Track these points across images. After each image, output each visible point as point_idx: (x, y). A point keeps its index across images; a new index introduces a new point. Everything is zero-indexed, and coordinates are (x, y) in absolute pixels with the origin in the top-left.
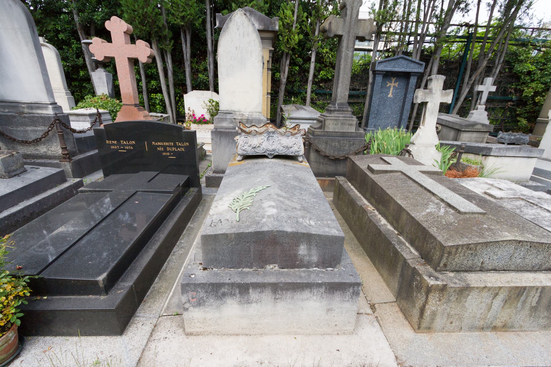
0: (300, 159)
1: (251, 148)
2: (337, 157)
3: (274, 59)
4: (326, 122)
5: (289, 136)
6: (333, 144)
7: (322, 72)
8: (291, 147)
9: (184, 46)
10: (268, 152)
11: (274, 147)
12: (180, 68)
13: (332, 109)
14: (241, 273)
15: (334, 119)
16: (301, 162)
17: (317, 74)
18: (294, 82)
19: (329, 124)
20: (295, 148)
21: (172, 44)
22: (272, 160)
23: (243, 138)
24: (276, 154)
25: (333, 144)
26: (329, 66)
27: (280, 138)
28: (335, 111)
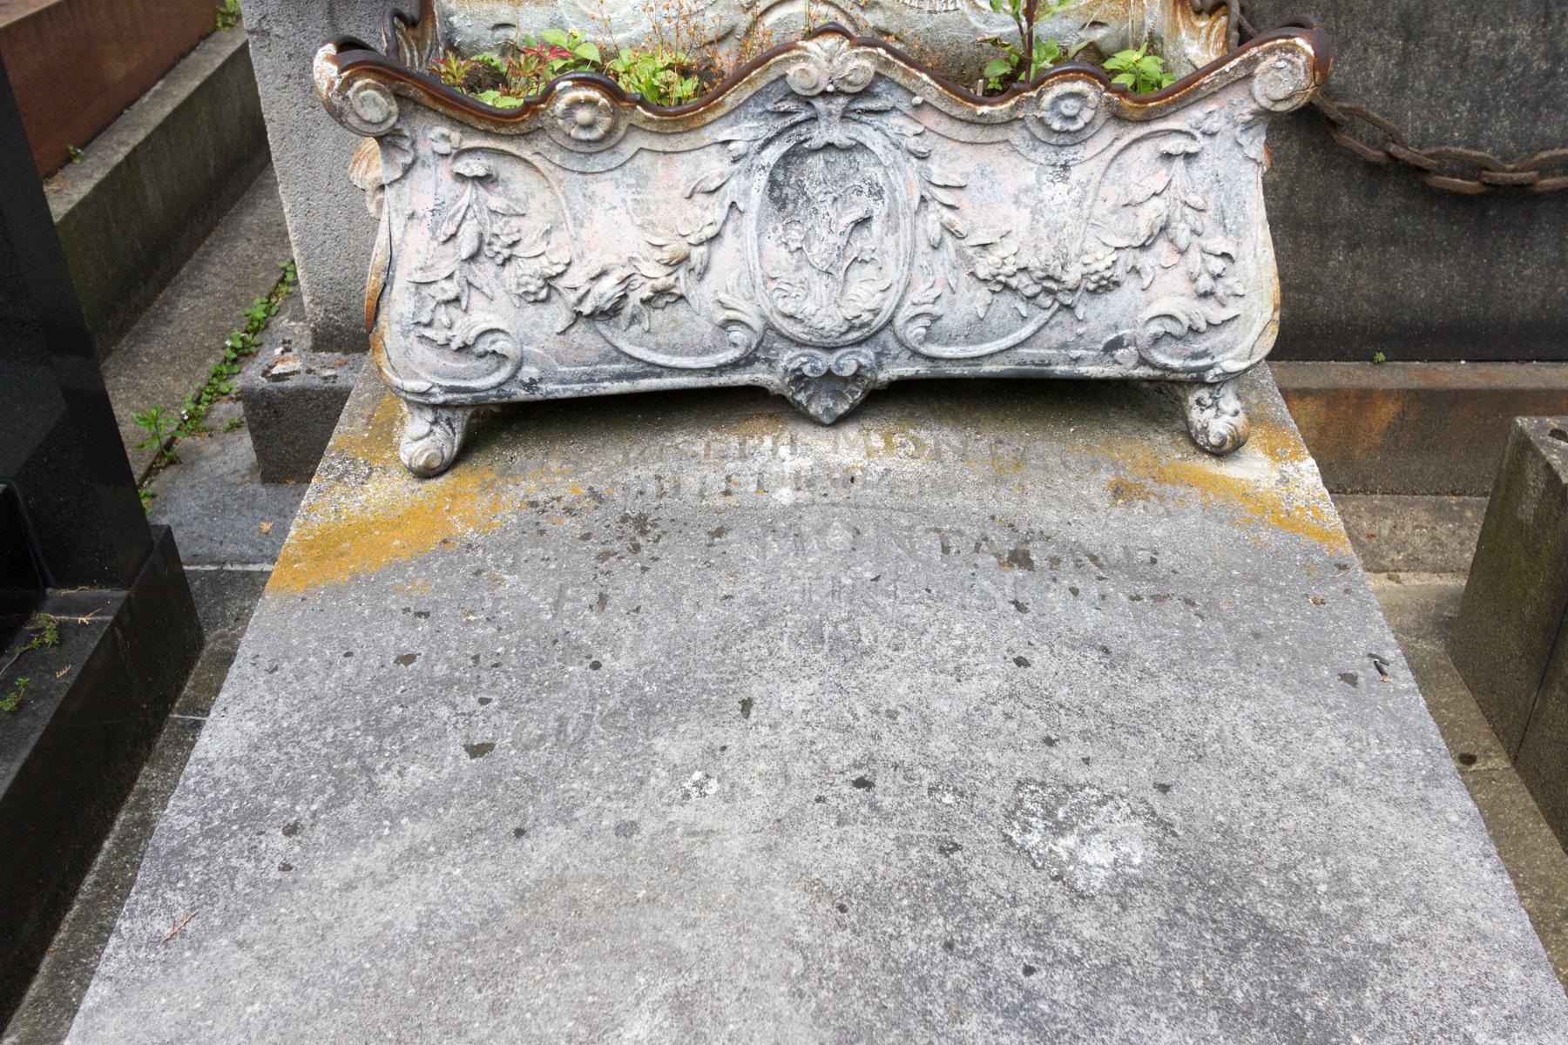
0: (1218, 418)
1: (557, 315)
2: (1506, 175)
5: (1076, 138)
6: (1483, 40)
8: (1106, 286)
10: (789, 358)
11: (864, 295)
14: (749, 82)
16: (1224, 451)
23: (431, 186)
25: (1483, 40)
27: (955, 161)
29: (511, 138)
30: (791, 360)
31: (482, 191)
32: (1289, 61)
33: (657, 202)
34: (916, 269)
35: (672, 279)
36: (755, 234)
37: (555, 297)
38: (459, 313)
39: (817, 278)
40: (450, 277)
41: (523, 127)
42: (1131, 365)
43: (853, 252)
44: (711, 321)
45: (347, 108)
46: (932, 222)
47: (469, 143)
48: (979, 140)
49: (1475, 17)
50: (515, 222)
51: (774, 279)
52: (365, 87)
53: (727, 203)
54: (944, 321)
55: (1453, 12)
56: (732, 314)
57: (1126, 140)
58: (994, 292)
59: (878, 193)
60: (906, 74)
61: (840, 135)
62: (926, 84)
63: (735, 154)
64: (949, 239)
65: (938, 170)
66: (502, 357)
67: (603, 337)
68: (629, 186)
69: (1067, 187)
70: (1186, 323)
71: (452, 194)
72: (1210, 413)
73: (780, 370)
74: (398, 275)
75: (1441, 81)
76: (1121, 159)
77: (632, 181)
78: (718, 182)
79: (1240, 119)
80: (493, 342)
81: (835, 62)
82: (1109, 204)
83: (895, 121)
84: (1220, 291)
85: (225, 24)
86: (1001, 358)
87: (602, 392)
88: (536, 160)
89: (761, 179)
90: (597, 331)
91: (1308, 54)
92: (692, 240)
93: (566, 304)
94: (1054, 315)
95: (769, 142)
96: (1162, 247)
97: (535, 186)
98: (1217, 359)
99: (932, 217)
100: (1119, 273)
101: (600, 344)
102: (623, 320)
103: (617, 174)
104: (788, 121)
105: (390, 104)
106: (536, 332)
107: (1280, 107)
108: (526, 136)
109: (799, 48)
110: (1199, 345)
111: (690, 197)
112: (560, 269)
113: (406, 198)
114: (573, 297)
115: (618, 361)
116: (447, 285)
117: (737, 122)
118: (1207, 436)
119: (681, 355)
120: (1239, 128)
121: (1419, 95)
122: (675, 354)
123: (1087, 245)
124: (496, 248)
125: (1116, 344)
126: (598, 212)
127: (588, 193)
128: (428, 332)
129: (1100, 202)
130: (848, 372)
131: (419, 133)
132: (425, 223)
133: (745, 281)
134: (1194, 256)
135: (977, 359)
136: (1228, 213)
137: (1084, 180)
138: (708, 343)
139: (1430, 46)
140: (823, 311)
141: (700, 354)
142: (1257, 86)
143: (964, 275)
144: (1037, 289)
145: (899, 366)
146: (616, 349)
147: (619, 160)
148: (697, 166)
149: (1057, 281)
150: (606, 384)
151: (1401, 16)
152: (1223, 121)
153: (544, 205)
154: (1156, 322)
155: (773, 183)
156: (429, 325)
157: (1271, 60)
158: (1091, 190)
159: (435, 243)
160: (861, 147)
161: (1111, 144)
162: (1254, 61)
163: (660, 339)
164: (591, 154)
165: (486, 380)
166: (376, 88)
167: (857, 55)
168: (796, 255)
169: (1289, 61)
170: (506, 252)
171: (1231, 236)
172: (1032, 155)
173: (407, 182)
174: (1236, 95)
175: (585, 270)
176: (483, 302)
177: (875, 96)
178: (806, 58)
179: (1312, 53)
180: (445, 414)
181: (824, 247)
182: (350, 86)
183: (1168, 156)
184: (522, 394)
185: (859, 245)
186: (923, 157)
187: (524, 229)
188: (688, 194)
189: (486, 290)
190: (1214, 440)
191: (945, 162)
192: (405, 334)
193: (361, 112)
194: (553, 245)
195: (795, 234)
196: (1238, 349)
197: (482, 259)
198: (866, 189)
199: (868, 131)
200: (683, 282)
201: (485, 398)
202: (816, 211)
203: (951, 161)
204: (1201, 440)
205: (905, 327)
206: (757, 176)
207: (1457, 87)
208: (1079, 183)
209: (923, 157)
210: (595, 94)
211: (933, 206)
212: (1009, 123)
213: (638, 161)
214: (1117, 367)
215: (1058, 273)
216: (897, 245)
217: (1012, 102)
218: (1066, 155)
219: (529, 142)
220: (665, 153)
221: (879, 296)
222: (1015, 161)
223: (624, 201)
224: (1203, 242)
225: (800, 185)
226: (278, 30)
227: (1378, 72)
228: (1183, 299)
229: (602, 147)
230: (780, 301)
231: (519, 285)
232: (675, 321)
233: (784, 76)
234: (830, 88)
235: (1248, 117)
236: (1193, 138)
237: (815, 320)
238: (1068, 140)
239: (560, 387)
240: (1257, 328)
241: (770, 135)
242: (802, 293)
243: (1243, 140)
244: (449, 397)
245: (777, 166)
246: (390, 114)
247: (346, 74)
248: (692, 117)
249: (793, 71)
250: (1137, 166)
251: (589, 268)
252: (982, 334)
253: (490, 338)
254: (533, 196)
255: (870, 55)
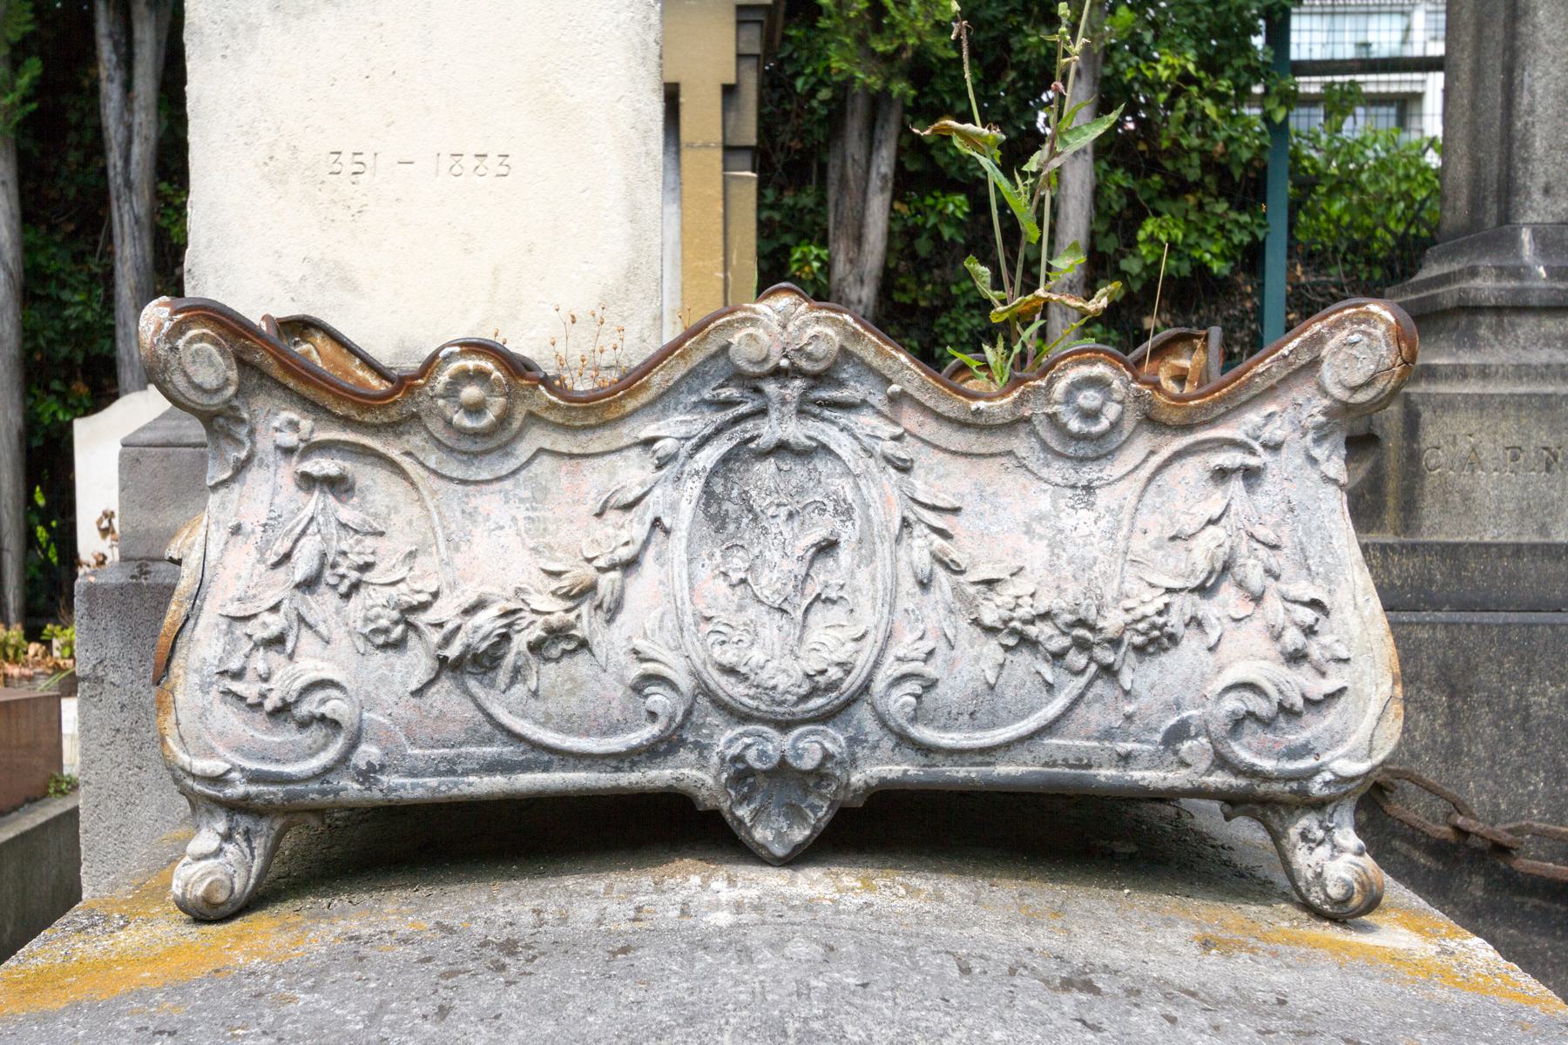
1: (415, 664)
3: (778, 158)
4: (1430, 435)
5: (1094, 447)
7: (1150, 226)
8: (1157, 642)
9: (111, 92)
10: (726, 739)
11: (830, 643)
12: (79, 258)
13: (1486, 286)
15: (1520, 402)
16: (1346, 912)
17: (1110, 245)
18: (932, 313)
19: (1473, 462)
20: (1236, 653)
21: (24, 81)
22: (813, 883)
24: (882, 767)
26: (1199, 185)
27: (940, 478)
28: (1519, 308)
29: (376, 429)
30: (731, 742)
31: (331, 499)
32: (1364, 333)
33: (557, 520)
34: (899, 614)
35: (572, 616)
36: (684, 558)
37: (413, 639)
38: (282, 659)
39: (766, 618)
40: (275, 609)
41: (393, 412)
42: (1204, 766)
43: (813, 589)
44: (621, 680)
45: (174, 363)
46: (920, 548)
47: (320, 436)
48: (975, 449)
49: (1528, 671)
50: (370, 542)
51: (708, 619)
52: (201, 338)
53: (649, 518)
54: (941, 689)
55: (1500, 664)
56: (650, 667)
57: (1165, 453)
58: (1007, 648)
59: (845, 512)
60: (879, 352)
61: (795, 431)
62: (903, 367)
63: (660, 454)
64: (941, 574)
65: (921, 486)
66: (335, 725)
67: (474, 699)
68: (522, 500)
69: (1092, 515)
70: (1275, 696)
71: (293, 506)
72: (1323, 852)
73: (715, 759)
74: (206, 607)
75: (1502, 747)
76: (1159, 480)
77: (526, 494)
78: (638, 491)
79: (1309, 423)
80: (323, 702)
81: (791, 328)
82: (1151, 536)
83: (865, 422)
84: (1314, 651)
85: (56, 791)
86: (1023, 753)
87: (467, 790)
88: (406, 463)
89: (694, 487)
90: (466, 691)
91: (1386, 322)
92: (601, 563)
93: (427, 651)
94: (1089, 685)
95: (705, 441)
96: (1228, 592)
97: (400, 498)
98: (1324, 758)
99: (917, 543)
100: (1175, 621)
101: (469, 711)
102: (502, 677)
103: (508, 484)
104: (731, 413)
105: (229, 367)
106: (382, 692)
107: (1361, 397)
108: (394, 428)
109: (745, 310)
110: (1296, 736)
111: (599, 515)
112: (424, 598)
113: (232, 507)
114: (436, 637)
115: (490, 741)
116: (268, 617)
117: (664, 413)
118: (1324, 887)
119: (579, 735)
120: (1310, 437)
121: (1479, 762)
122: (569, 732)
123: (1126, 586)
124: (341, 570)
125: (1179, 733)
126: (479, 533)
127: (469, 509)
128: (236, 687)
129: (1138, 534)
130: (809, 763)
131: (261, 414)
132: (252, 539)
133: (670, 624)
134: (1273, 604)
135: (987, 753)
136: (1311, 551)
137: (1114, 506)
138: (616, 714)
139: (1481, 704)
140: (775, 663)
141: (604, 734)
142: (1327, 374)
143: (964, 624)
144: (1066, 641)
145: (880, 762)
146: (490, 718)
147: (512, 464)
148: (612, 474)
149: (1092, 628)
150: (472, 779)
151: (1439, 668)
152: (1288, 428)
153: (410, 523)
154: (1233, 694)
155: (708, 493)
156: (238, 675)
157: (1341, 335)
158: (1125, 518)
159: (262, 568)
160: (825, 449)
161: (1145, 461)
162: (1318, 340)
163: (552, 707)
164: (476, 455)
165: (304, 759)
166: (216, 343)
167: (818, 320)
168: (740, 590)
169: (1364, 333)
170: (354, 575)
171: (1318, 581)
172: (1044, 473)
173: (236, 487)
174: (1302, 392)
175: (456, 602)
176: (318, 646)
177: (841, 384)
178: (754, 322)
179: (1392, 320)
180: (244, 822)
181: (776, 575)
182: (182, 333)
183: (1222, 475)
184: (351, 788)
185: (822, 578)
186: (904, 468)
187: (380, 552)
188: (597, 510)
189: (322, 628)
190: (1335, 892)
191: (931, 478)
192: (204, 688)
193: (190, 370)
194: (417, 571)
195: (738, 562)
196: (1352, 741)
197: (322, 588)
198: (830, 507)
199: (833, 431)
200: (587, 622)
201: (303, 795)
202: (765, 532)
203: (939, 477)
204: (1315, 897)
205: (887, 693)
206: (689, 484)
207: (1523, 753)
208: (1109, 510)
209: (904, 468)
210: (488, 365)
211: (919, 530)
212: (1013, 425)
213: (536, 467)
214: (1184, 772)
215: (1092, 615)
216: (873, 579)
217: (1015, 394)
218: (1089, 473)
219: (399, 435)
220: (571, 456)
221: (851, 646)
222: (1022, 480)
223: (514, 519)
224: (1284, 588)
225: (745, 498)
226: (114, 677)
227: (1423, 734)
228: (1265, 664)
229: (491, 444)
230: (717, 648)
231: (367, 620)
232: (572, 679)
233: (725, 349)
234: (784, 363)
235: (1321, 419)
236: (1252, 452)
237: (764, 675)
238: (1087, 450)
239: (408, 781)
240: (1374, 709)
241: (707, 431)
242: (747, 638)
243: (1317, 452)
244: (253, 789)
245: (714, 472)
246: (227, 382)
247: (180, 316)
248: (609, 404)
249: (736, 338)
250: (1182, 490)
251: (462, 599)
252: (993, 712)
253: (319, 695)
254: (397, 511)
255: (834, 321)
